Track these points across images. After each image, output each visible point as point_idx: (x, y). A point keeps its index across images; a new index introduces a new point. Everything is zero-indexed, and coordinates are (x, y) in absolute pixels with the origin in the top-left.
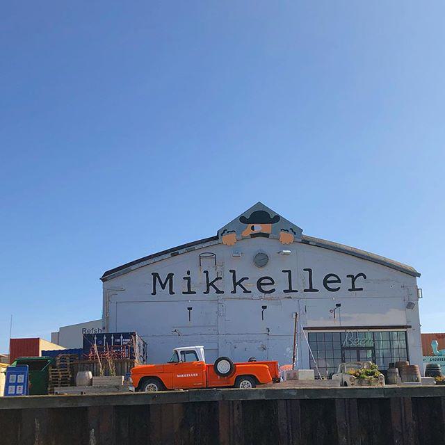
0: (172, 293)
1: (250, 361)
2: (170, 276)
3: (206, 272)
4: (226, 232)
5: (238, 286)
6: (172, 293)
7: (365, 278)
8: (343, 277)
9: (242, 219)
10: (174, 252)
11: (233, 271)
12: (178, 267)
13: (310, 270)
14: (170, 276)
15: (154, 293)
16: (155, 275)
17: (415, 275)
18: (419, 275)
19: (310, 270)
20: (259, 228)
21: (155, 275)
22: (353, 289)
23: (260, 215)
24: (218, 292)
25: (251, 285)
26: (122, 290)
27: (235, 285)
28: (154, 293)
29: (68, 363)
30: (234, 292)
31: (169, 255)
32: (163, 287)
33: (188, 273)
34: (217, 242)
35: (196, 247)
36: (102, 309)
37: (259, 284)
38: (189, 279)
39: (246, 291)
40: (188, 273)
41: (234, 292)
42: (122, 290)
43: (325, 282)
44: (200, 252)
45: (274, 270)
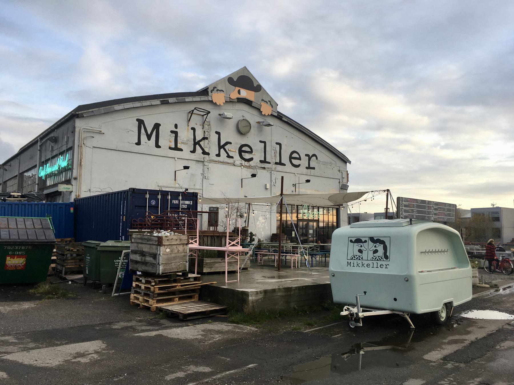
0: (157, 146)
1: (226, 217)
2: (157, 126)
3: (193, 129)
4: (215, 89)
5: (222, 150)
6: (157, 146)
7: (317, 158)
8: (303, 156)
9: (230, 80)
10: (164, 99)
11: (218, 133)
12: (167, 118)
13: (265, 143)
14: (157, 126)
15: (139, 143)
16: (141, 122)
17: (344, 160)
18: (350, 162)
19: (265, 143)
20: (244, 93)
21: (141, 122)
22: (309, 168)
23: (244, 80)
24: (204, 153)
25: (233, 150)
26: (100, 133)
27: (220, 147)
28: (139, 143)
29: (143, 287)
30: (218, 155)
31: (157, 102)
32: (149, 137)
33: (176, 126)
34: (204, 98)
35: (188, 99)
36: (37, 136)
37: (241, 151)
38: (176, 133)
39: (229, 156)
40: (176, 126)
41: (218, 155)
42: (100, 133)
43: (291, 158)
44: (191, 107)
45: (252, 139)
